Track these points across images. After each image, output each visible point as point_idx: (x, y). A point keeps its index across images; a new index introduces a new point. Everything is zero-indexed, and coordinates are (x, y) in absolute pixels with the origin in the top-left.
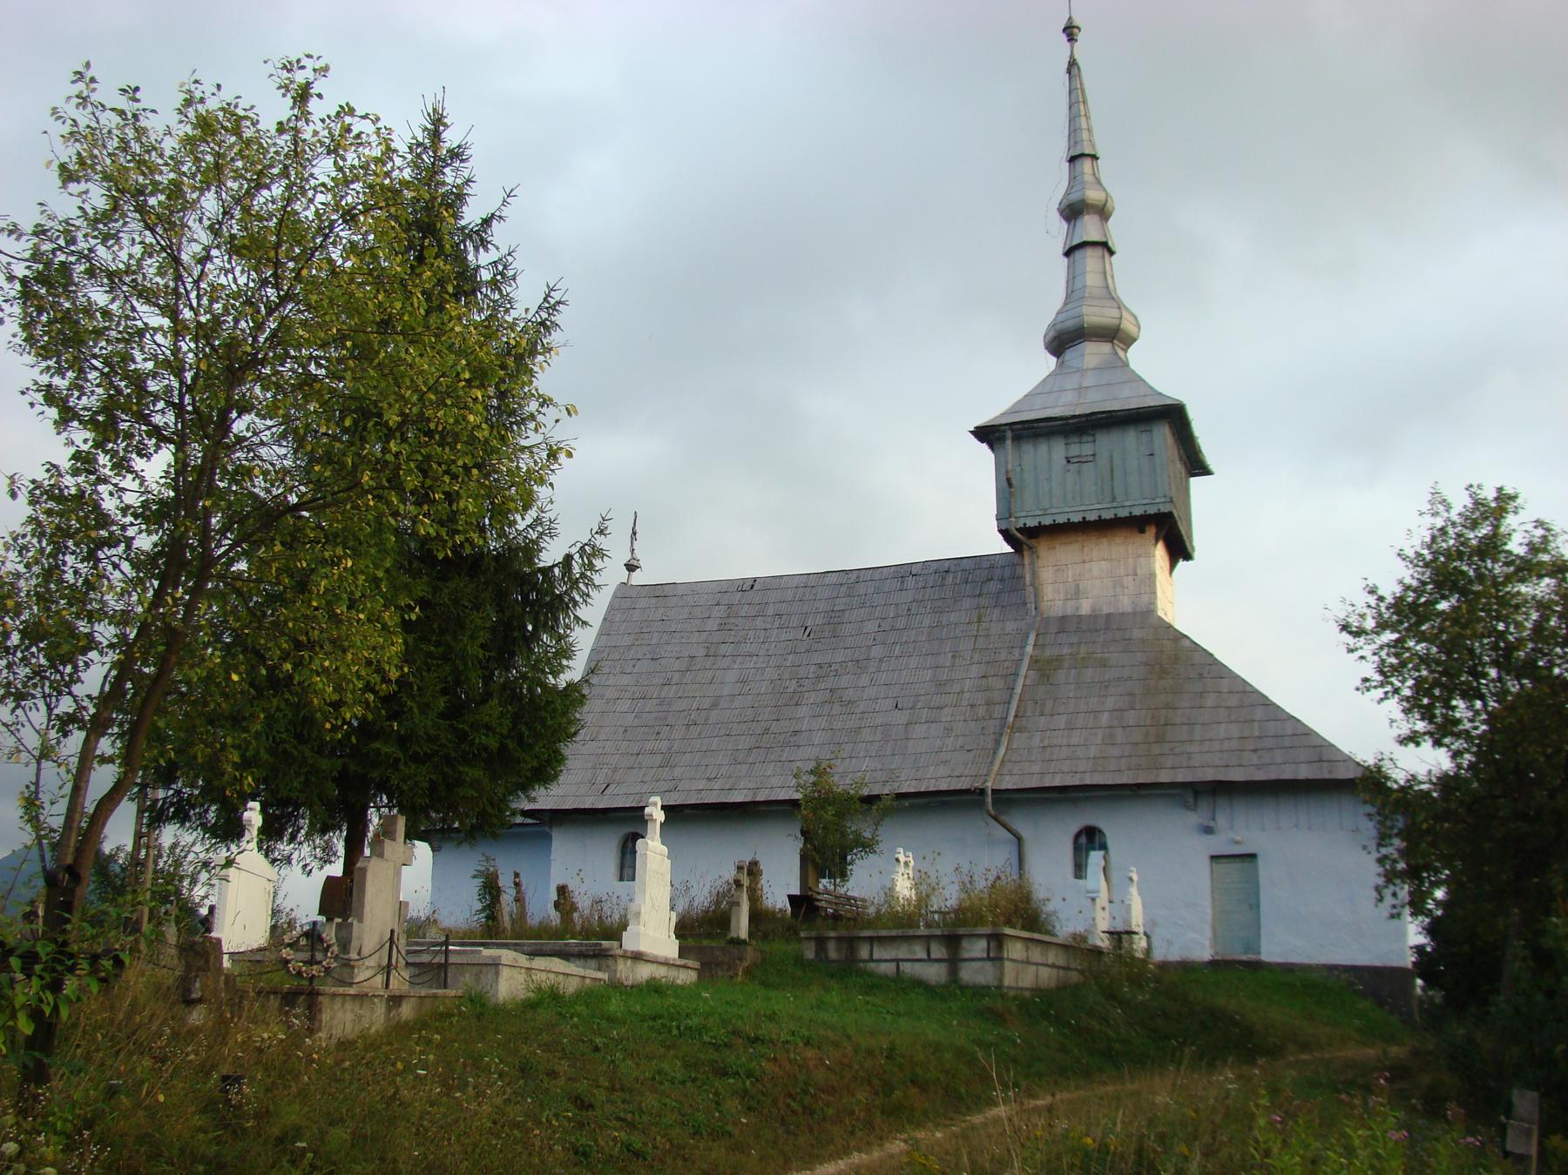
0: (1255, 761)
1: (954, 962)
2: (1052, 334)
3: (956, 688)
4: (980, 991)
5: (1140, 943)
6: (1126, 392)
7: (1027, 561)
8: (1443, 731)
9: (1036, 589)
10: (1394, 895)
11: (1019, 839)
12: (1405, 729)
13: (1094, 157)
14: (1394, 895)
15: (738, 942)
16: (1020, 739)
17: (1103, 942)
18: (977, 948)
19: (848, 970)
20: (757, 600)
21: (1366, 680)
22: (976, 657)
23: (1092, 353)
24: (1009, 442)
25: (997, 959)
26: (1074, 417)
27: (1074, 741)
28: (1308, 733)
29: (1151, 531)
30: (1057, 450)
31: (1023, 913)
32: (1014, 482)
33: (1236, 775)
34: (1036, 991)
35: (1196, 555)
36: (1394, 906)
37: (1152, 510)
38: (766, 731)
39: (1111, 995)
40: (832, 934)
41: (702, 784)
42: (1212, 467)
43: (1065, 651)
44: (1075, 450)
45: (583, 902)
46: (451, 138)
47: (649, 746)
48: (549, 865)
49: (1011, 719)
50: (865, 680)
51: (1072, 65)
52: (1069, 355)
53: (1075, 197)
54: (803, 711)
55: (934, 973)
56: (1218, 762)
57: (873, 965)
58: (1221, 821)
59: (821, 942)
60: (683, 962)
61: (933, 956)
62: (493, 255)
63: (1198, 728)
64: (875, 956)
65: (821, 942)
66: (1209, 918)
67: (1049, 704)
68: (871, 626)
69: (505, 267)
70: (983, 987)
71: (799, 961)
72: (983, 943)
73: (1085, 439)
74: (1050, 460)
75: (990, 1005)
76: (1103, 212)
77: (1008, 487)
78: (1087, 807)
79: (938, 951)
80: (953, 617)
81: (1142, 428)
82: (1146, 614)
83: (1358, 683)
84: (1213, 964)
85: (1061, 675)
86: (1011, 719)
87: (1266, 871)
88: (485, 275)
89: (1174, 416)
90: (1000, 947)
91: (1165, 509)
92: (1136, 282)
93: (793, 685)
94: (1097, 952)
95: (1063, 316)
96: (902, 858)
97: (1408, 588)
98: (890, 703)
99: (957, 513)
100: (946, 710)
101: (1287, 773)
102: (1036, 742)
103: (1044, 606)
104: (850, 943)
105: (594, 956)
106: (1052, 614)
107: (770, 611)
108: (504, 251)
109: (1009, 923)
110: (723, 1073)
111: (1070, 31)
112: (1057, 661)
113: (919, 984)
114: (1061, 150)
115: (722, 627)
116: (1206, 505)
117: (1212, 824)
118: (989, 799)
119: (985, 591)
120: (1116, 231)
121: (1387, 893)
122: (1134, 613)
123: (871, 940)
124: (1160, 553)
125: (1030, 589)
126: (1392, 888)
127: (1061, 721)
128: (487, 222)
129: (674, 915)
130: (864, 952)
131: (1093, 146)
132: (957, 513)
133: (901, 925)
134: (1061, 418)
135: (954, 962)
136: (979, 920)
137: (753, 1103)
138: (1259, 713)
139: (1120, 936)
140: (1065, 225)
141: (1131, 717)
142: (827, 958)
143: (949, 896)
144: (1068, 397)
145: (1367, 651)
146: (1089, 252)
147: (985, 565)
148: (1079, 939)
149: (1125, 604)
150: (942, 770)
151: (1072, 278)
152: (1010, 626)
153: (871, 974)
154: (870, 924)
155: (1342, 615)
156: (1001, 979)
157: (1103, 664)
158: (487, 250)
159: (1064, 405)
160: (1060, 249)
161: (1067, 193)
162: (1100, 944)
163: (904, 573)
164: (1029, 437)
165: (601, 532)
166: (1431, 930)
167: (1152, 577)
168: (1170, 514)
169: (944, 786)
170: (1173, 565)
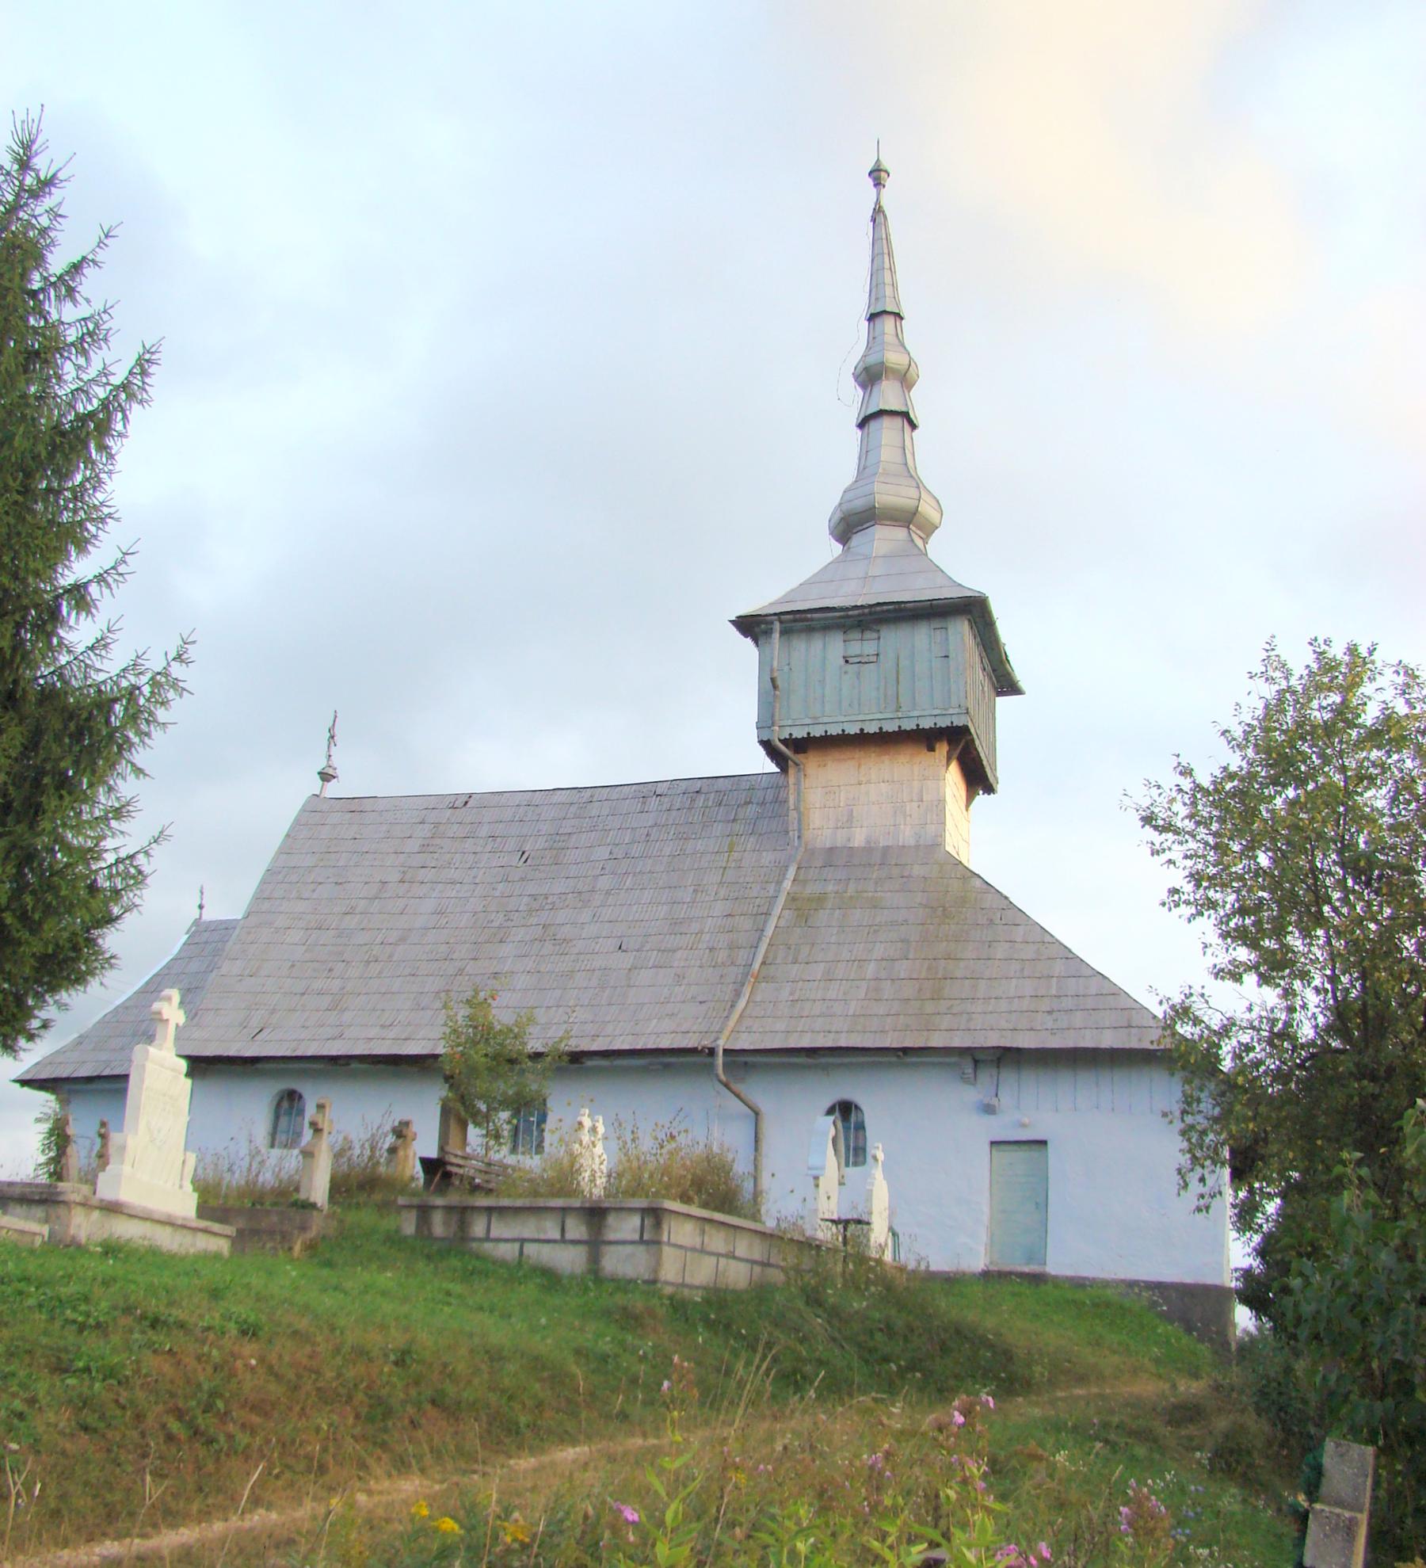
0: (1049, 1025)
1: (595, 1244)
2: (838, 515)
3: (695, 927)
4: (624, 1285)
5: (879, 1233)
7: (792, 780)
8: (1275, 967)
9: (799, 813)
10: (1202, 1180)
11: (757, 1114)
12: (1223, 960)
13: (898, 316)
14: (1202, 1180)
16: (765, 991)
17: (826, 1234)
20: (468, 819)
21: (1174, 891)
22: (722, 893)
23: (882, 539)
24: (776, 635)
26: (856, 607)
27: (831, 994)
28: (1117, 992)
29: (942, 749)
30: (834, 647)
31: (717, 1192)
32: (779, 683)
35: (999, 788)
36: (1202, 1196)
37: (943, 723)
38: (460, 972)
39: (814, 1299)
40: (439, 1201)
41: (374, 1032)
42: (1022, 685)
43: (830, 888)
44: (855, 648)
46: (42, 164)
47: (317, 985)
48: (124, 1104)
49: (756, 966)
50: (585, 916)
51: (878, 213)
52: (856, 540)
53: (872, 360)
54: (507, 950)
55: (569, 1259)
56: (1004, 1024)
57: (488, 1246)
58: (1006, 1099)
60: (203, 1224)
61: (569, 1236)
62: (84, 311)
63: (982, 984)
64: (494, 1233)
66: (985, 1218)
67: (805, 950)
68: (602, 853)
69: (97, 326)
70: (630, 1281)
72: (635, 1220)
73: (868, 635)
74: (824, 659)
75: (632, 1308)
76: (906, 380)
77: (772, 687)
79: (577, 1229)
80: (700, 845)
81: (936, 623)
82: (932, 847)
83: (1164, 895)
84: (986, 1275)
85: (822, 917)
86: (756, 966)
88: (72, 335)
90: (658, 1225)
91: (958, 722)
93: (499, 919)
94: (809, 1246)
95: (851, 495)
96: (587, 1122)
97: (1231, 776)
100: (679, 954)
101: (1087, 1041)
102: (785, 994)
103: (808, 835)
104: (462, 1214)
105: (42, 1202)
106: (818, 845)
107: (484, 831)
108: (98, 306)
111: (877, 175)
112: (820, 900)
114: (862, 310)
115: (425, 849)
116: (1010, 730)
117: (994, 1101)
118: (720, 1059)
119: (741, 815)
120: (920, 403)
121: (1193, 1178)
122: (917, 847)
123: (490, 1210)
124: (953, 778)
125: (793, 814)
126: (1199, 1170)
127: (818, 970)
128: (76, 268)
129: (192, 1159)
130: (478, 1228)
131: (898, 305)
134: (842, 609)
135: (595, 1244)
137: (92, 1419)
138: (1059, 968)
139: (853, 1225)
140: (861, 392)
141: (903, 969)
142: (430, 1233)
145: (1177, 853)
146: (886, 422)
147: (744, 785)
149: (907, 835)
151: (865, 452)
152: (767, 858)
155: (1146, 802)
156: (656, 1271)
157: (875, 905)
158: (75, 302)
160: (853, 416)
161: (864, 356)
162: (820, 1235)
163: (648, 793)
164: (801, 631)
165: (179, 658)
166: (1262, 1252)
167: (940, 804)
168: (965, 730)
169: (665, 1043)
170: (970, 798)
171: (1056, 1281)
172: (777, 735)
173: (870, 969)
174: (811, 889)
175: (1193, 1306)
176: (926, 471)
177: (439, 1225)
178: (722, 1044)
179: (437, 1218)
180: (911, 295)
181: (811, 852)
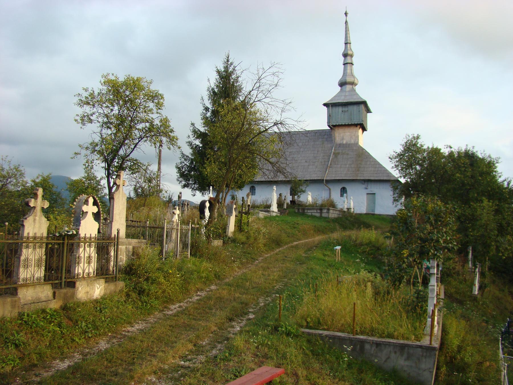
1: (321, 213)
4: (326, 218)
5: (352, 210)
6: (355, 97)
15: (284, 209)
17: (346, 210)
18: (325, 211)
19: (303, 214)
23: (348, 87)
25: (328, 212)
29: (359, 126)
30: (340, 109)
31: (332, 205)
33: (372, 178)
34: (334, 218)
37: (359, 123)
39: (347, 219)
43: (340, 151)
45: (183, 198)
46: (231, 61)
52: (343, 87)
53: (345, 52)
55: (318, 215)
58: (369, 187)
59: (298, 209)
65: (298, 209)
71: (295, 212)
75: (327, 220)
76: (352, 56)
77: (329, 116)
78: (344, 184)
79: (319, 211)
82: (357, 144)
84: (366, 214)
85: (339, 156)
87: (377, 197)
89: (364, 103)
91: (362, 123)
92: (358, 71)
94: (345, 212)
98: (305, 161)
99: (320, 122)
102: (334, 170)
104: (304, 209)
109: (330, 207)
110: (295, 228)
111: (346, 14)
112: (339, 153)
113: (315, 216)
116: (371, 120)
124: (360, 131)
130: (306, 211)
132: (320, 122)
133: (313, 206)
136: (325, 206)
138: (378, 166)
139: (348, 209)
140: (343, 58)
141: (353, 166)
143: (320, 202)
144: (343, 97)
146: (348, 65)
148: (342, 209)
149: (353, 142)
150: (315, 175)
152: (329, 145)
153: (307, 215)
154: (306, 206)
157: (348, 154)
159: (342, 100)
160: (342, 63)
167: (358, 137)
170: (363, 132)
171: (377, 215)
172: (331, 124)
173: (348, 166)
174: (337, 151)
175: (93, 296)
176: (355, 73)
177: (300, 211)
178: (325, 179)
179: (300, 210)
180: (352, 39)
181: (337, 145)
